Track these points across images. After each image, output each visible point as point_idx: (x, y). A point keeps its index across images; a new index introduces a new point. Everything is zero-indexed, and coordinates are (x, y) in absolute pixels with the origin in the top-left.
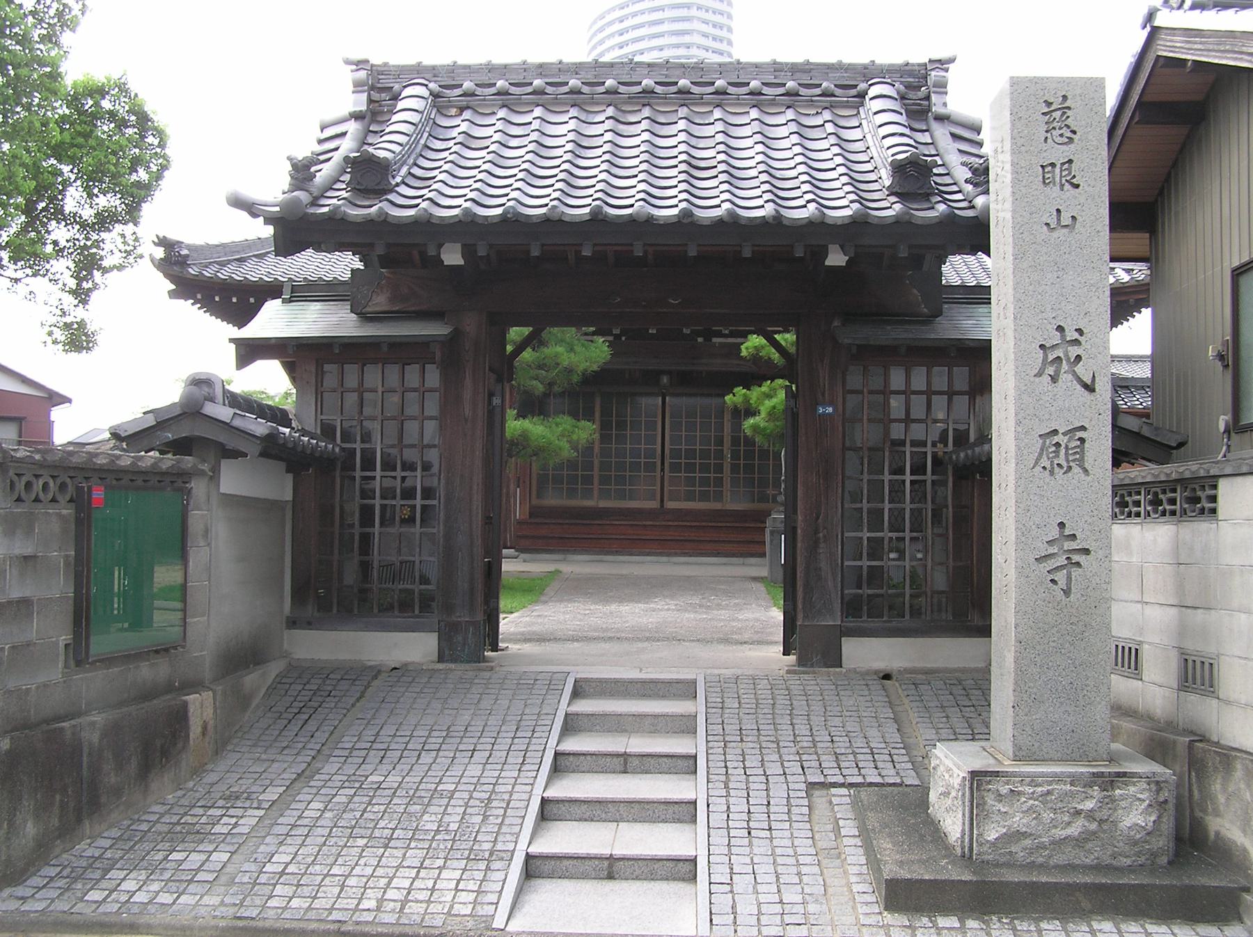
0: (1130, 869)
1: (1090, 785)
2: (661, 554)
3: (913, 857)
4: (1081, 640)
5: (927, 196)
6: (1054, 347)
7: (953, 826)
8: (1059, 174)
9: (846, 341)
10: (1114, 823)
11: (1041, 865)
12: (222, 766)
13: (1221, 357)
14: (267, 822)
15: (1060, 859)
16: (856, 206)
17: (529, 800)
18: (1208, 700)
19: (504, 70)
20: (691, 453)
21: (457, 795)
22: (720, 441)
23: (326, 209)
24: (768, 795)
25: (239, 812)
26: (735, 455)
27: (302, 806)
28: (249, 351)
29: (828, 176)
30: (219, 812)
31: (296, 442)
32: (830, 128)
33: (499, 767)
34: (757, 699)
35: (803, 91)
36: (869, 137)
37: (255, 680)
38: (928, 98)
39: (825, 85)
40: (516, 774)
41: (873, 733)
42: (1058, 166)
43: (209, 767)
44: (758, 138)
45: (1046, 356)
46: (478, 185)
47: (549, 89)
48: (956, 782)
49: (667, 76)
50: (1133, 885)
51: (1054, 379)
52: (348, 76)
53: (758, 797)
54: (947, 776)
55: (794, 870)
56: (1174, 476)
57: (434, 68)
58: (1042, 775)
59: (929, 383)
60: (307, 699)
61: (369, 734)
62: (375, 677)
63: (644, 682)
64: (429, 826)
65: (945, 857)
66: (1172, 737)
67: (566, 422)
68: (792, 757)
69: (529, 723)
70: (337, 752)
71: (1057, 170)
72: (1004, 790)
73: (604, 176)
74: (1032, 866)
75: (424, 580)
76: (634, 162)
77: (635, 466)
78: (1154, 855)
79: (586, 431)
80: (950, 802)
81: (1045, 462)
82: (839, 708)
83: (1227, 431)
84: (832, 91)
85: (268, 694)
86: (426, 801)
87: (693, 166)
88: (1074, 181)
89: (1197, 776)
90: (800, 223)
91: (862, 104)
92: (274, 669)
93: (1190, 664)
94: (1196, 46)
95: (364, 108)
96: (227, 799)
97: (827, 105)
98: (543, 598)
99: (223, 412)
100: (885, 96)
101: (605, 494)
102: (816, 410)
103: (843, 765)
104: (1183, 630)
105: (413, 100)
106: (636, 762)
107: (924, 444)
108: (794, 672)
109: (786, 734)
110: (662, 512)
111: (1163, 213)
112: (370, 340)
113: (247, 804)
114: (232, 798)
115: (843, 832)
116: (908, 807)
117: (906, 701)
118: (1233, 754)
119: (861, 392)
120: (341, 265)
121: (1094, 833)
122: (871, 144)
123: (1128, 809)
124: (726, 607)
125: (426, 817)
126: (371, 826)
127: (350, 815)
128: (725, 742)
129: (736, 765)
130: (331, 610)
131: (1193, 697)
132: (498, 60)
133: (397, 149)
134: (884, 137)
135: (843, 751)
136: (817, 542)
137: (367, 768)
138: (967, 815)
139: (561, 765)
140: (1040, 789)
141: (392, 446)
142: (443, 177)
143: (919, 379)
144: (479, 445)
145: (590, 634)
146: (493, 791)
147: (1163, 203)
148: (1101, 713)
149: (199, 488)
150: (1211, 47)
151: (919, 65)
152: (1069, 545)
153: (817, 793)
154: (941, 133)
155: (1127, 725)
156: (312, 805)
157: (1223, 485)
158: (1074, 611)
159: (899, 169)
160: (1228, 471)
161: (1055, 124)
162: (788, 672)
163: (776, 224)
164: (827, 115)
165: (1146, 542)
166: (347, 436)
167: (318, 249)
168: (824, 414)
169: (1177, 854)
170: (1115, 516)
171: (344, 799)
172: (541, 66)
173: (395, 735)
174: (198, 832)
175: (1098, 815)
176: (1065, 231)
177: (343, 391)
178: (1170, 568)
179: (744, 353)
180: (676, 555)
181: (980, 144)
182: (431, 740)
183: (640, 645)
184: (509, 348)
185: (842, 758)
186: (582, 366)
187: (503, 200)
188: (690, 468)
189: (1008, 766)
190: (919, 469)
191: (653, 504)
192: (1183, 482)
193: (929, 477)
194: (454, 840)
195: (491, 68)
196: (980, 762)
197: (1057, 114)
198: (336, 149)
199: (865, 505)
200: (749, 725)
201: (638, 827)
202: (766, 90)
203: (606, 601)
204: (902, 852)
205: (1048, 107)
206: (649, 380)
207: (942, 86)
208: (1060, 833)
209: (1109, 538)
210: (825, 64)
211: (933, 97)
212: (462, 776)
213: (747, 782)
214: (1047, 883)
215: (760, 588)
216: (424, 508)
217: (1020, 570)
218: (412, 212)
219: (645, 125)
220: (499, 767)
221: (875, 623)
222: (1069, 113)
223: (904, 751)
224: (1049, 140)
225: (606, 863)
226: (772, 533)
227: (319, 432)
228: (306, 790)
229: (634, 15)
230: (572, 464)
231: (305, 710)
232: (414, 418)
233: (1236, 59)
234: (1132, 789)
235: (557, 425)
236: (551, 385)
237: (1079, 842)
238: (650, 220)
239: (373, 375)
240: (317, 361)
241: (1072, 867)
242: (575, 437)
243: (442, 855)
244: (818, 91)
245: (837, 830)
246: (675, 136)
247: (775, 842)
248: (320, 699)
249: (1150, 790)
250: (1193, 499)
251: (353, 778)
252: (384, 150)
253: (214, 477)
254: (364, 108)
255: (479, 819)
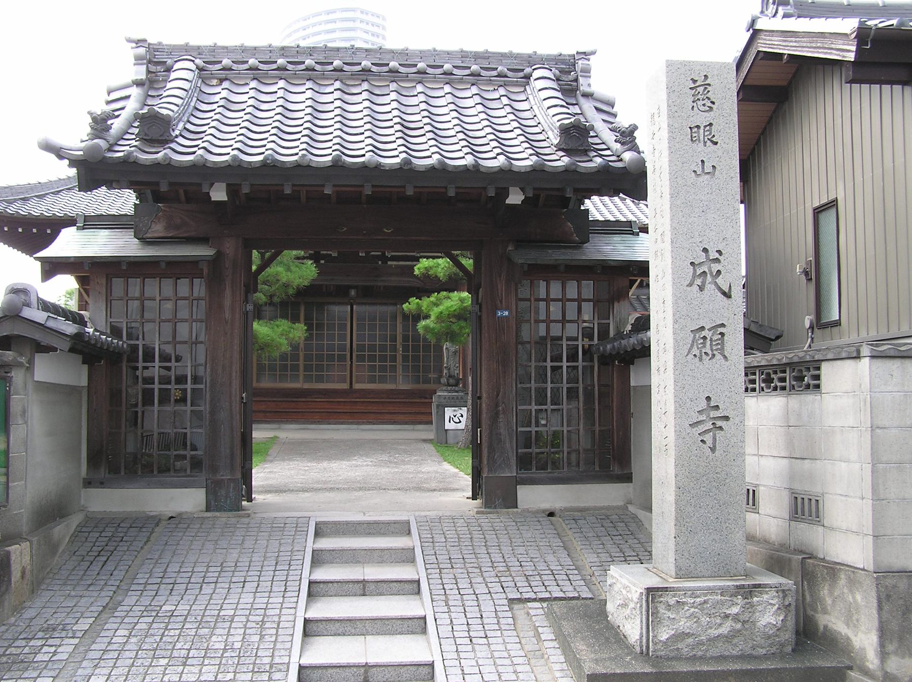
0: (766, 657)
1: (734, 595)
2: (352, 423)
3: (604, 656)
4: (717, 486)
5: (585, 152)
6: (701, 264)
7: (633, 630)
8: (702, 134)
9: (520, 261)
10: (754, 623)
11: (701, 658)
12: (39, 602)
13: (806, 273)
14: (82, 649)
15: (714, 652)
16: (534, 158)
17: (294, 621)
18: (815, 527)
19: (255, 50)
20: (372, 348)
21: (236, 619)
22: (394, 339)
23: (121, 154)
24: (480, 610)
25: (58, 641)
26: (406, 348)
27: (110, 633)
28: (52, 268)
29: (517, 135)
30: (40, 643)
31: (97, 340)
32: (505, 100)
33: (267, 594)
34: (458, 535)
35: (483, 73)
36: (535, 107)
37: (63, 530)
38: (576, 80)
39: (500, 68)
40: (281, 600)
41: (550, 558)
42: (702, 128)
43: (28, 604)
44: (452, 107)
45: (695, 271)
46: (241, 138)
47: (290, 67)
48: (635, 597)
49: (380, 59)
50: (770, 670)
51: (701, 288)
52: (129, 53)
53: (473, 612)
54: (624, 592)
55: (511, 669)
56: (784, 361)
57: (199, 47)
58: (700, 589)
59: (579, 293)
60: (104, 544)
61: (158, 571)
62: (157, 525)
63: (369, 523)
64: (217, 646)
65: (628, 654)
66: (787, 555)
67: (284, 324)
68: (493, 580)
69: (286, 558)
70: (134, 587)
71: (701, 131)
72: (672, 601)
73: (338, 133)
74: (694, 659)
75: (194, 448)
76: (360, 123)
77: (331, 358)
78: (782, 645)
79: (299, 331)
80: (628, 612)
81: (695, 351)
82: (521, 540)
83: (812, 327)
84: (507, 73)
85: (71, 541)
86: (212, 624)
87: (405, 127)
88: (714, 139)
89: (810, 587)
90: (494, 170)
91: (528, 84)
92: (75, 521)
93: (799, 500)
94: (791, 44)
95: (144, 77)
96: (45, 631)
97: (502, 83)
98: (269, 458)
99: (40, 316)
100: (545, 78)
101: (308, 379)
102: (496, 314)
103: (533, 584)
104: (792, 476)
105: (183, 73)
106: (372, 587)
107: (576, 339)
108: (482, 513)
109: (485, 562)
110: (351, 391)
111: (754, 170)
112: (152, 260)
113: (64, 634)
114: (50, 630)
115: (543, 637)
116: (591, 615)
117: (570, 533)
118: (838, 567)
119: (529, 300)
120: (124, 201)
121: (739, 631)
122: (537, 113)
123: (763, 612)
124: (409, 463)
125: (214, 638)
126: (170, 647)
127: (151, 640)
128: (440, 569)
129: (451, 586)
130: (120, 472)
131: (802, 525)
132: (250, 43)
133: (175, 108)
134: (548, 108)
135: (531, 573)
136: (497, 414)
137: (160, 599)
138: (644, 622)
139: (315, 590)
140: (698, 600)
141: (168, 343)
142: (213, 131)
143: (572, 290)
144: (237, 341)
145: (316, 486)
146: (265, 615)
147: (754, 160)
148: (738, 537)
149: (18, 376)
150: (805, 45)
151: (569, 56)
152: (713, 414)
153: (516, 607)
154: (588, 106)
155: (751, 547)
156: (119, 633)
157: (825, 368)
158: (718, 463)
159: (565, 131)
160: (830, 356)
161: (699, 96)
162: (478, 513)
163: (474, 171)
164: (502, 91)
165: (765, 411)
166: (130, 336)
167: (110, 187)
168: (502, 317)
169: (797, 644)
170: (746, 390)
171: (144, 626)
172: (283, 48)
173: (179, 572)
174: (22, 661)
175: (741, 618)
176: (707, 176)
177: (127, 298)
178: (782, 429)
179: (417, 272)
180: (363, 423)
181: (615, 116)
182: (208, 575)
183: (357, 494)
184: (254, 268)
185: (531, 578)
186: (295, 284)
187: (263, 150)
188: (372, 358)
189: (672, 583)
190: (572, 357)
191: (345, 386)
192: (791, 365)
193: (580, 363)
194: (239, 657)
195: (244, 49)
196: (654, 581)
197: (701, 89)
198: (123, 108)
199: (533, 385)
200: (455, 555)
201: (381, 638)
202: (455, 71)
203: (319, 459)
204: (595, 652)
205: (695, 85)
206: (340, 293)
207: (587, 71)
208: (714, 632)
209: (743, 408)
210: (500, 53)
211: (581, 79)
212: (238, 603)
213: (462, 600)
214: (708, 671)
215: (430, 447)
216: (193, 390)
217: (678, 433)
218: (191, 158)
219: (365, 95)
220: (267, 594)
221: (542, 474)
222: (709, 88)
223: (576, 572)
224: (695, 108)
225: (362, 670)
226: (438, 406)
227: (109, 331)
228: (112, 620)
229: (314, 25)
230: (284, 357)
231: (108, 554)
232: (186, 321)
233: (826, 53)
234: (766, 596)
235: (277, 326)
236: (271, 296)
237: (728, 638)
238: (378, 167)
239: (152, 287)
240: (107, 275)
241: (722, 658)
242: (291, 335)
243: (231, 669)
244: (495, 73)
245: (538, 635)
246: (389, 102)
247: (493, 647)
248: (115, 544)
249: (778, 596)
250: (802, 377)
251: (150, 608)
252: (167, 106)
253: (30, 368)
254: (144, 77)
255: (256, 638)
